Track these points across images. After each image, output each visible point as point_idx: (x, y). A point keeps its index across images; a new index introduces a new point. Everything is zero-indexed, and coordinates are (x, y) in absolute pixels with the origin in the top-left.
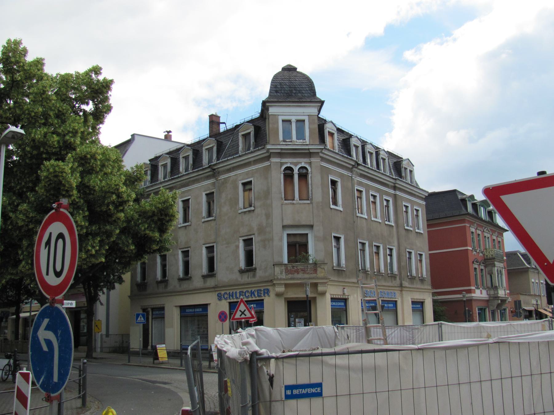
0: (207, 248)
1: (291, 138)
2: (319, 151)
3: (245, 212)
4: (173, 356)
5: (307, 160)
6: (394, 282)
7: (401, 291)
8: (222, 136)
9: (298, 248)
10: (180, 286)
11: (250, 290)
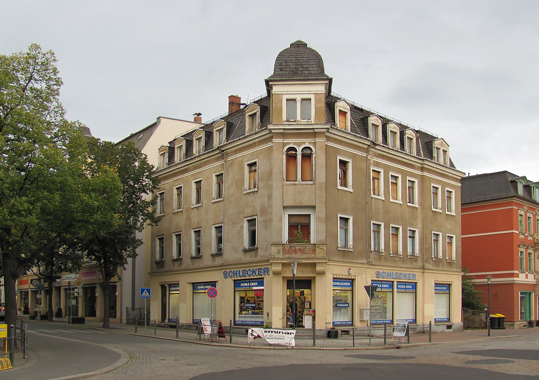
2: (325, 130)
4: (185, 329)
5: (311, 140)
6: (414, 264)
7: (423, 272)
9: (300, 228)
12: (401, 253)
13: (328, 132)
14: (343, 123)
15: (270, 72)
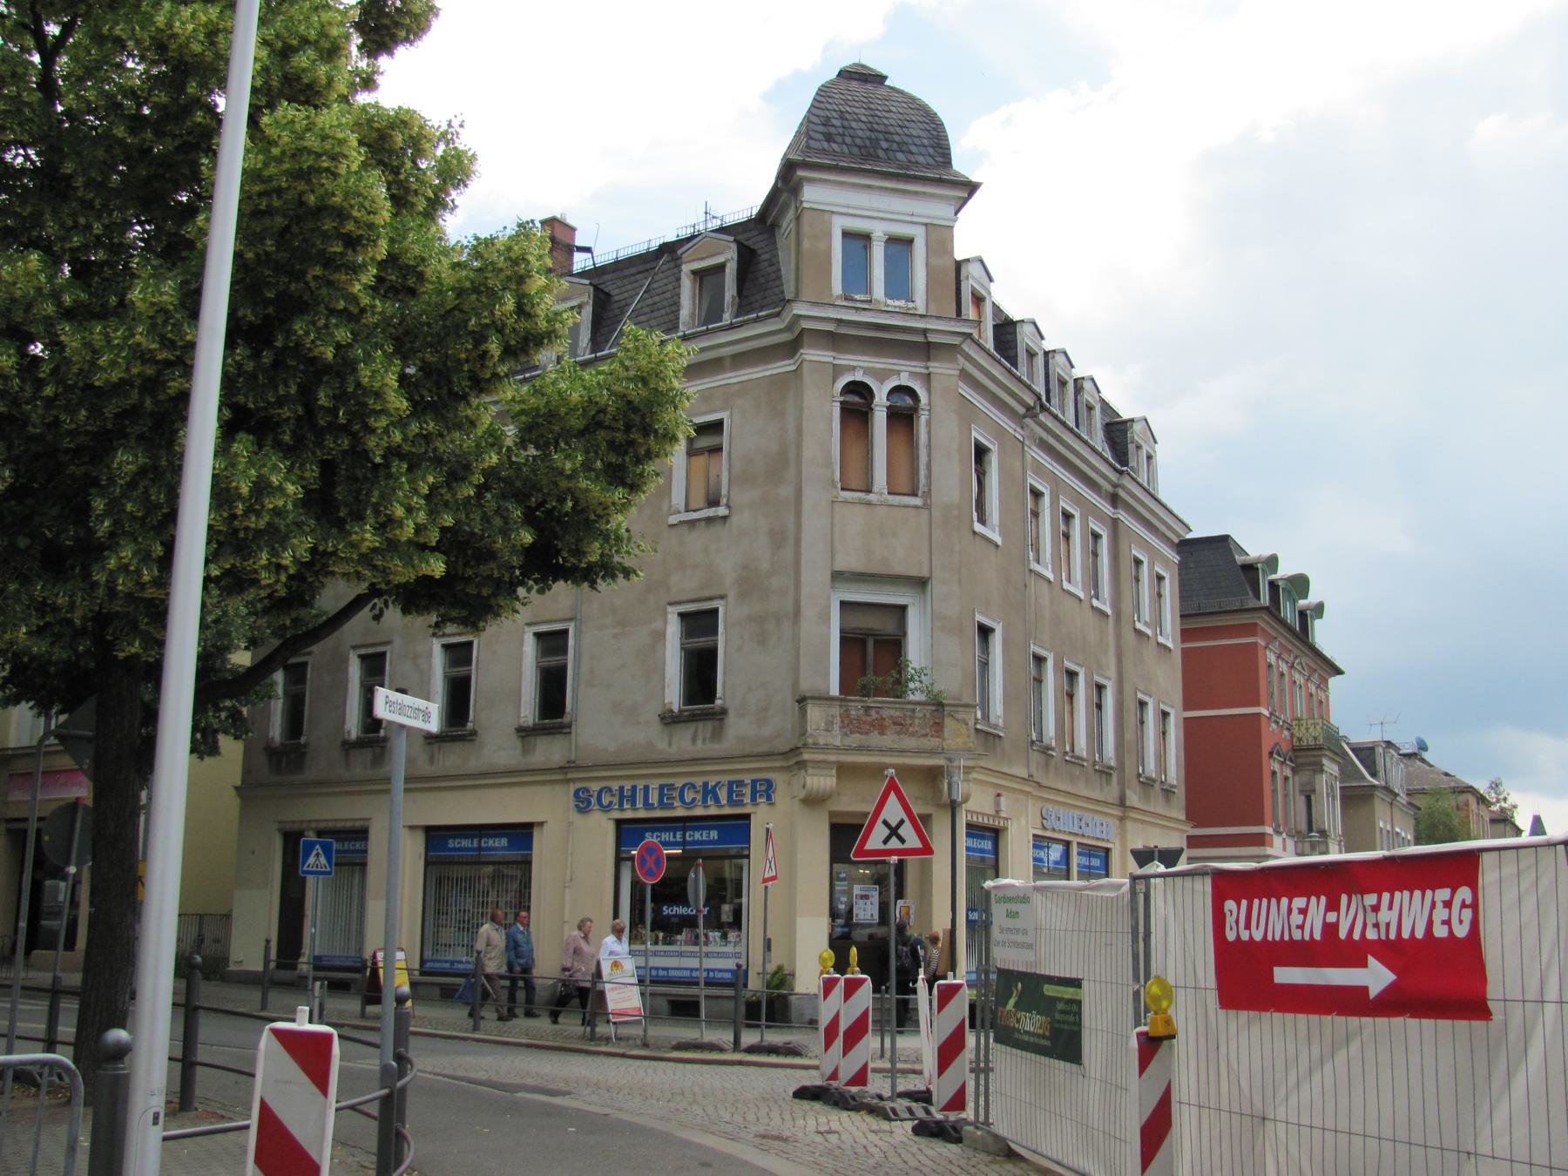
0: (539, 636)
1: (868, 289)
2: (956, 340)
3: (692, 523)
5: (917, 366)
7: (1122, 819)
8: (606, 277)
9: (873, 651)
10: (432, 760)
11: (699, 782)
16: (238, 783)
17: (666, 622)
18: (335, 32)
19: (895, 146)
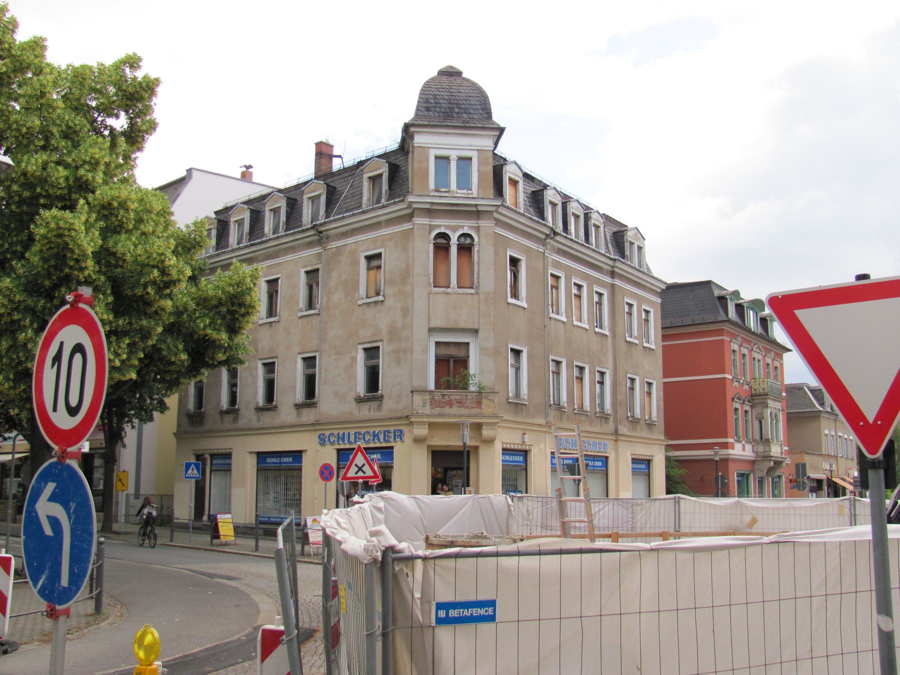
1: (448, 185)
2: (493, 209)
3: (368, 304)
5: (473, 223)
6: (605, 426)
7: (616, 441)
9: (452, 366)
12: (588, 409)
13: (497, 211)
14: (516, 197)
15: (408, 114)
16: (175, 431)
17: (357, 353)
18: (97, 156)
19: (462, 111)
